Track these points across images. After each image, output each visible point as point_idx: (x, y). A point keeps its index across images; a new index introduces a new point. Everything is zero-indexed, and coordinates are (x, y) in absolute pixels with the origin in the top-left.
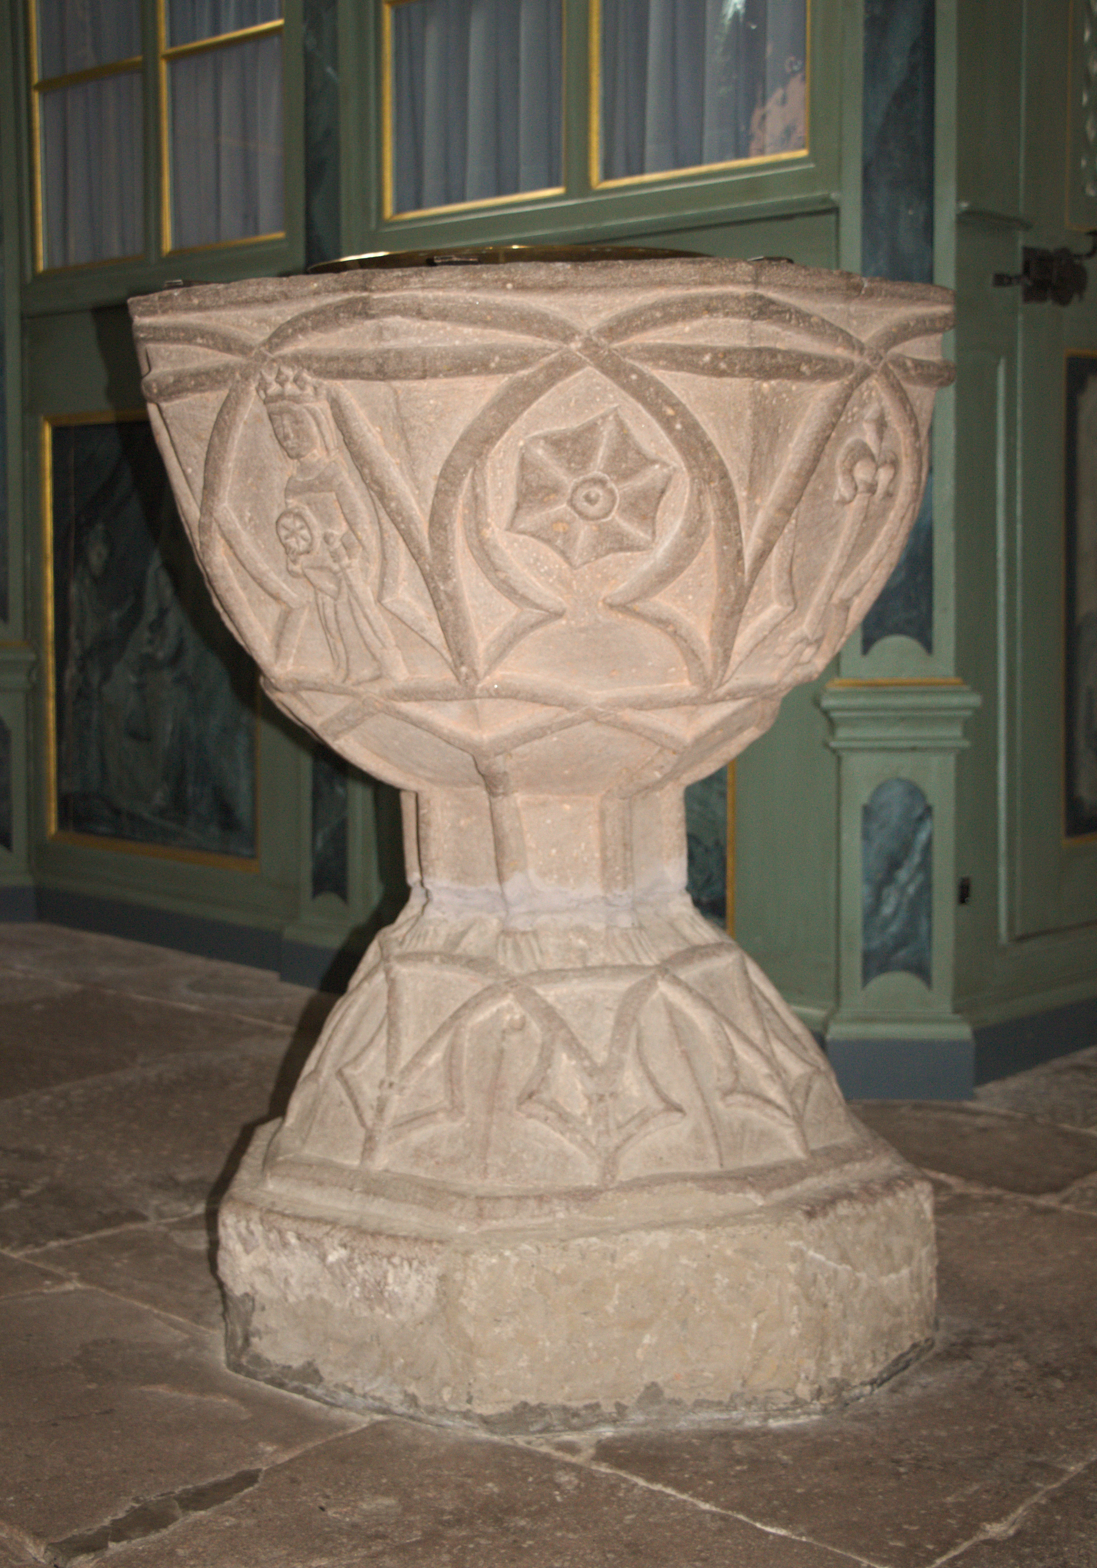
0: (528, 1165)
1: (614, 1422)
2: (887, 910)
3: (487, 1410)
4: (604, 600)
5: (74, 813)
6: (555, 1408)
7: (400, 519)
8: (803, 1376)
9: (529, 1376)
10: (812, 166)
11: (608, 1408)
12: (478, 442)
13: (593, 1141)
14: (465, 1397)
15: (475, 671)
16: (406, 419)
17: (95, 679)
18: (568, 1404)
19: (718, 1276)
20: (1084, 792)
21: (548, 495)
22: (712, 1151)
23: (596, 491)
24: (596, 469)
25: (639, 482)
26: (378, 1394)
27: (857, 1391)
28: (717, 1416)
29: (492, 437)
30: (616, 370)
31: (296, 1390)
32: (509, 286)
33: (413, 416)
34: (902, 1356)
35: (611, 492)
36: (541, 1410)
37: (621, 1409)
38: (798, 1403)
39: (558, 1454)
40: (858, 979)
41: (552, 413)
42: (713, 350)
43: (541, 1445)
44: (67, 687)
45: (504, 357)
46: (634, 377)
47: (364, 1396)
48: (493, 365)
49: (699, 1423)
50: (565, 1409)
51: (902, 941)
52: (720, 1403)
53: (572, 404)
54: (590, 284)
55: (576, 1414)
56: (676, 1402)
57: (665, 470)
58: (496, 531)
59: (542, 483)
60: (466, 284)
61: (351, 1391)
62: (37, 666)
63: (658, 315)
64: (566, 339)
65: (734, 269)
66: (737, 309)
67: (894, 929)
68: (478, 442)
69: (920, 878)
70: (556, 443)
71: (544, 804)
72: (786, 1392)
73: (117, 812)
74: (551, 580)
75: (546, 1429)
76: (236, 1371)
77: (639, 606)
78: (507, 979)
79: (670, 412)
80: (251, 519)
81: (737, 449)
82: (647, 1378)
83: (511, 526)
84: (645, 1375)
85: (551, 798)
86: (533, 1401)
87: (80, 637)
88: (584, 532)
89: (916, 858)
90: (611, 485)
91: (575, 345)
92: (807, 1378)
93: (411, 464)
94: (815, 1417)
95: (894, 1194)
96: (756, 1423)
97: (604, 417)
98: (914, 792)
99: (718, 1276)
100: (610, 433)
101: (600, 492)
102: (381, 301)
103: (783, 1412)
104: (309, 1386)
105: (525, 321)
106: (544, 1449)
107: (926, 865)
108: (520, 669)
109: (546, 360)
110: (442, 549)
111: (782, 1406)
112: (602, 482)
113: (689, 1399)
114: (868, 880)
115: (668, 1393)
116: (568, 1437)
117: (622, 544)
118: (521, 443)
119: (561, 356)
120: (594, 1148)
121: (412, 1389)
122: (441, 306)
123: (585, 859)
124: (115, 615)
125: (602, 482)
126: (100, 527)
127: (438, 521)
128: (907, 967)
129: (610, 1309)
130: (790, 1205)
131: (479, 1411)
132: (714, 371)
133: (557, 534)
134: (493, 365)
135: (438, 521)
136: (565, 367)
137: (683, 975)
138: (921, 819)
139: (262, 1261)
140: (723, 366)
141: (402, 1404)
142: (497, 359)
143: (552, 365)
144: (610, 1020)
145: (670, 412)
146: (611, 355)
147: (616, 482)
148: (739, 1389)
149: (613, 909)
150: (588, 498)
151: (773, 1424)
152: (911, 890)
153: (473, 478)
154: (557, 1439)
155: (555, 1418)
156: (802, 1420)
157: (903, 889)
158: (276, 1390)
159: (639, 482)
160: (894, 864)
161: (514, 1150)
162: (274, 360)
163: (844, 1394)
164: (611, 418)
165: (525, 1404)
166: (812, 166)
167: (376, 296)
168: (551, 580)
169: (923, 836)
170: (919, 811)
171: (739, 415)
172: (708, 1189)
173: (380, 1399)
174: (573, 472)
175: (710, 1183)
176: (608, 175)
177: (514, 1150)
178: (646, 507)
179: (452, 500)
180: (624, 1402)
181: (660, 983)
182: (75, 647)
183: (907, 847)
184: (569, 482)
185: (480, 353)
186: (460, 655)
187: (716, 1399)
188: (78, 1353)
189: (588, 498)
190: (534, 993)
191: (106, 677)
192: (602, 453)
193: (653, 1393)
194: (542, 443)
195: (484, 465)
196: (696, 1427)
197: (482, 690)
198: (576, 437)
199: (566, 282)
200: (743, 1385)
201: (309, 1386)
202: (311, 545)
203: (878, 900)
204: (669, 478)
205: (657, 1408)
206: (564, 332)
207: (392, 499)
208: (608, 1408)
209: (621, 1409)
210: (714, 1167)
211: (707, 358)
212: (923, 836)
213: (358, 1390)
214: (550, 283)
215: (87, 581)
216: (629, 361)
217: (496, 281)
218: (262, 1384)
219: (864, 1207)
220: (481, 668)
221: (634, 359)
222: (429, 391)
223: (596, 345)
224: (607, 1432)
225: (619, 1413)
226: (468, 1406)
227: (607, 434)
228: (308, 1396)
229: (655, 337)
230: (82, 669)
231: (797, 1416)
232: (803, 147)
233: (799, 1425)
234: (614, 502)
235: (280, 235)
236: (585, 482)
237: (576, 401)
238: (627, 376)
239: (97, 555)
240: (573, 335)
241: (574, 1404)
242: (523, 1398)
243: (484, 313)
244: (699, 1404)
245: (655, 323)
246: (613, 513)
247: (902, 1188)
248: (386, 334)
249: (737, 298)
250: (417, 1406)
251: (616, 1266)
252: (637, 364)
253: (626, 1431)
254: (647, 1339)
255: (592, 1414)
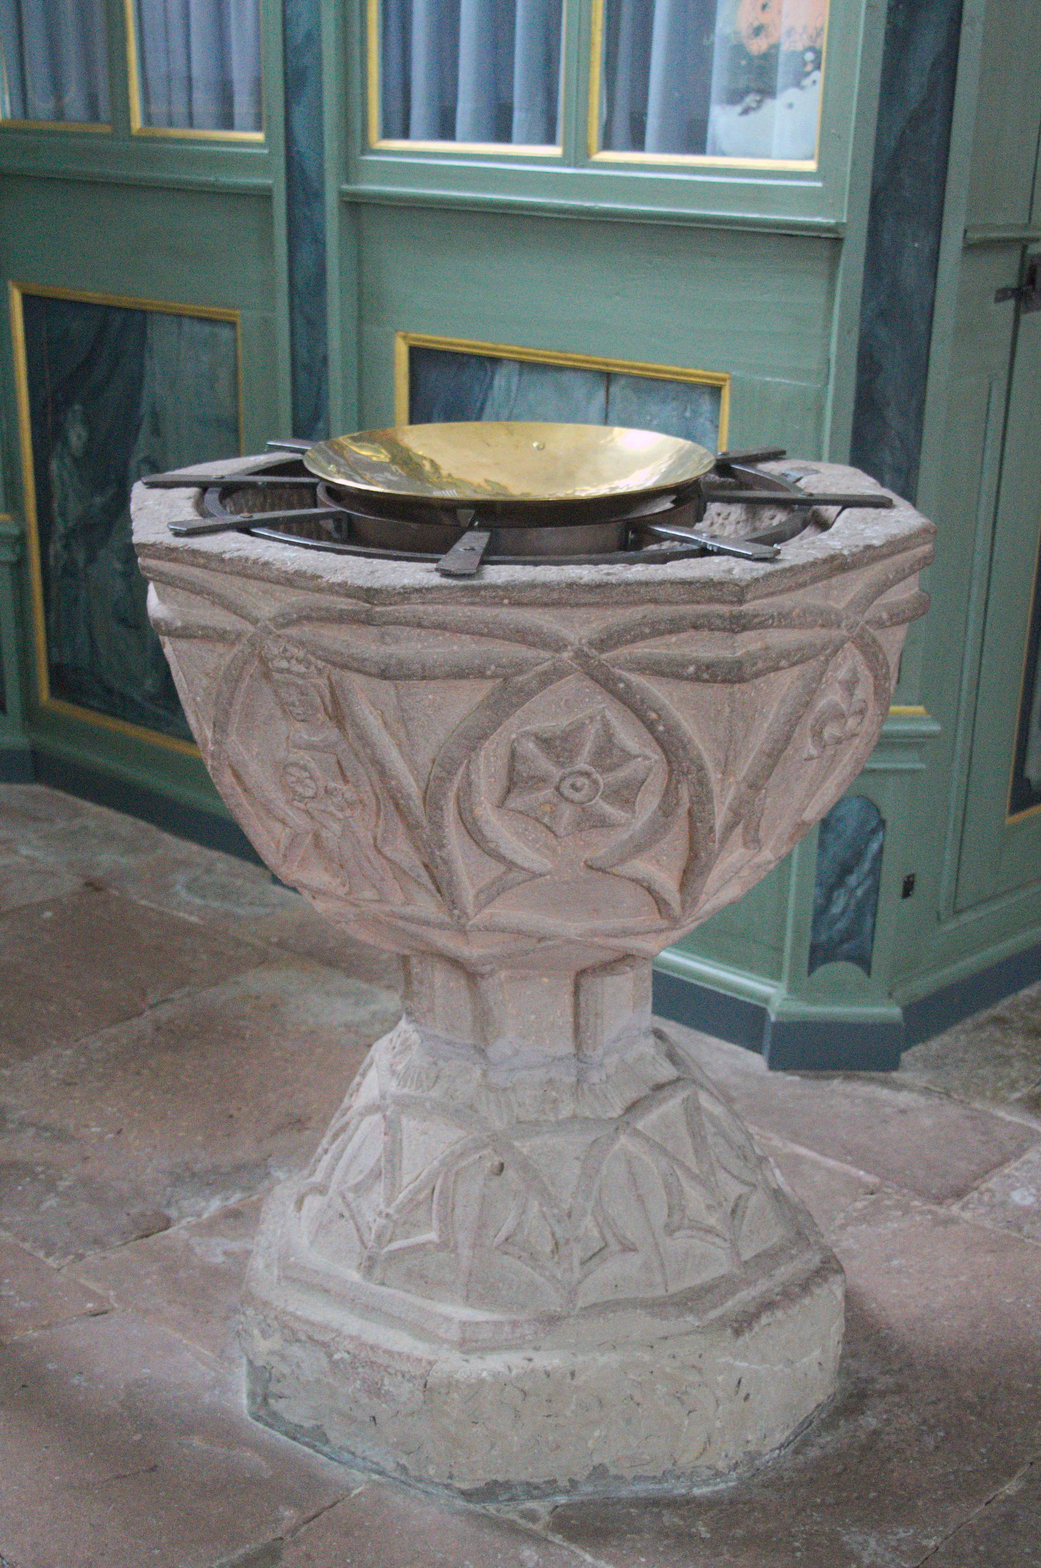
0: (504, 1293)
1: (568, 1492)
2: (836, 909)
3: (465, 1486)
4: (585, 862)
5: (62, 682)
6: (521, 1484)
7: (399, 795)
8: (723, 1454)
9: (500, 1461)
10: (819, 184)
11: (563, 1483)
12: (473, 739)
13: (559, 1276)
14: (447, 1475)
15: (466, 913)
16: (406, 711)
17: (81, 557)
18: (531, 1481)
19: (658, 1386)
20: (1032, 772)
21: (536, 783)
22: (658, 1278)
23: (581, 781)
24: (582, 763)
25: (621, 774)
26: (375, 1460)
27: (767, 1457)
28: (651, 1487)
29: (486, 734)
30: (605, 681)
31: (307, 1444)
32: (506, 601)
33: (413, 708)
34: (807, 1417)
35: (595, 782)
36: (507, 1485)
37: (574, 1484)
38: (718, 1474)
39: (521, 1522)
40: (806, 974)
41: (543, 715)
42: (696, 662)
43: (508, 1512)
44: (52, 562)
45: (498, 666)
46: (622, 685)
47: (364, 1459)
48: (489, 673)
49: (637, 1493)
50: (528, 1484)
51: (848, 935)
52: (655, 1477)
53: (562, 704)
54: (583, 601)
55: (537, 1488)
56: (618, 1477)
57: (647, 762)
58: (486, 812)
59: (532, 773)
60: (465, 600)
61: (353, 1453)
62: (21, 539)
63: (647, 631)
64: (558, 650)
65: (721, 590)
66: (722, 626)
67: (840, 925)
68: (473, 739)
69: (869, 882)
70: (545, 743)
71: (525, 979)
72: (708, 1468)
73: (109, 691)
74: (538, 846)
75: (512, 1499)
76: (257, 1420)
77: (619, 870)
78: (489, 1133)
79: (653, 716)
80: (258, 754)
81: (715, 740)
82: (596, 1460)
83: (501, 804)
84: (595, 1459)
85: (531, 972)
86: (500, 1478)
87: (63, 515)
88: (567, 812)
89: (866, 866)
90: (596, 776)
91: (565, 655)
92: (726, 1456)
93: (408, 748)
94: (731, 1484)
95: (812, 1293)
96: (683, 1491)
97: (592, 718)
98: (871, 806)
99: (658, 1386)
100: (597, 732)
101: (586, 781)
102: (382, 614)
103: (706, 1483)
104: (318, 1444)
105: (522, 636)
106: (512, 1516)
107: (875, 871)
108: (507, 912)
109: (539, 668)
110: (438, 826)
111: (704, 1477)
112: (587, 775)
113: (629, 1475)
114: (820, 884)
115: (613, 1471)
116: (530, 1505)
117: (603, 823)
118: (514, 736)
119: (554, 664)
120: (559, 1282)
121: (403, 1461)
122: (441, 620)
123: (561, 1023)
124: (98, 500)
125: (587, 775)
126: (77, 407)
127: (432, 800)
128: (849, 958)
129: (568, 1413)
130: (722, 1322)
131: (458, 1485)
132: (696, 678)
133: (545, 813)
134: (489, 673)
135: (432, 800)
136: (557, 673)
137: (640, 1125)
138: (874, 831)
139: (277, 1347)
140: (706, 676)
141: (395, 1471)
142: (493, 667)
143: (545, 673)
144: (576, 1167)
145: (653, 716)
146: (601, 665)
147: (601, 774)
148: (670, 1466)
149: (584, 1066)
150: (573, 786)
151: (697, 1491)
152: (859, 893)
153: (467, 767)
154: (521, 1507)
155: (520, 1491)
156: (722, 1486)
157: (852, 891)
158: (290, 1442)
159: (621, 774)
160: (846, 870)
161: (491, 1280)
162: (279, 636)
163: (757, 1462)
164: (598, 718)
165: (496, 1482)
166: (819, 184)
167: (378, 609)
168: (538, 846)
169: (875, 846)
170: (873, 823)
171: (719, 712)
172: (654, 1315)
173: (378, 1464)
174: (560, 764)
175: (656, 1309)
176: (607, 144)
177: (491, 1280)
178: (625, 795)
179: (448, 785)
180: (577, 1478)
181: (622, 1137)
182: (60, 527)
183: (858, 856)
184: (556, 773)
185: (477, 661)
186: (453, 902)
187: (651, 1475)
188: (122, 1397)
189: (573, 786)
190: (513, 1147)
191: (91, 559)
192: (588, 748)
193: (599, 1472)
194: (533, 738)
195: (478, 756)
196: (634, 1495)
197: (472, 926)
198: (565, 737)
199: (561, 599)
200: (674, 1464)
201: (318, 1444)
202: (316, 793)
203: (829, 900)
204: (650, 769)
205: (604, 1482)
206: (558, 645)
207: (392, 778)
208: (563, 1483)
209: (574, 1484)
210: (660, 1292)
211: (691, 669)
212: (875, 846)
213: (358, 1452)
214: (545, 599)
215: (68, 461)
216: (617, 671)
217: (494, 597)
218: (278, 1435)
219: (785, 1313)
220: (470, 910)
221: (624, 670)
222: (427, 694)
223: (587, 656)
224: (562, 1499)
225: (572, 1486)
226: (449, 1481)
227: (592, 731)
228: (317, 1451)
229: (642, 649)
230: (66, 547)
231: (716, 1484)
232: (811, 158)
233: (717, 1492)
234: (598, 790)
235: (259, 137)
236: (571, 773)
237: (567, 701)
238: (615, 684)
239: (76, 436)
240: (566, 646)
241: (535, 1480)
242: (494, 1477)
243: (481, 626)
244: (637, 1478)
245: (644, 637)
246: (597, 798)
247: (819, 1285)
248: (388, 639)
249: (721, 617)
250: (407, 1474)
251: (574, 1383)
252: (626, 674)
253: (577, 1498)
254: (597, 1434)
255: (551, 1486)
